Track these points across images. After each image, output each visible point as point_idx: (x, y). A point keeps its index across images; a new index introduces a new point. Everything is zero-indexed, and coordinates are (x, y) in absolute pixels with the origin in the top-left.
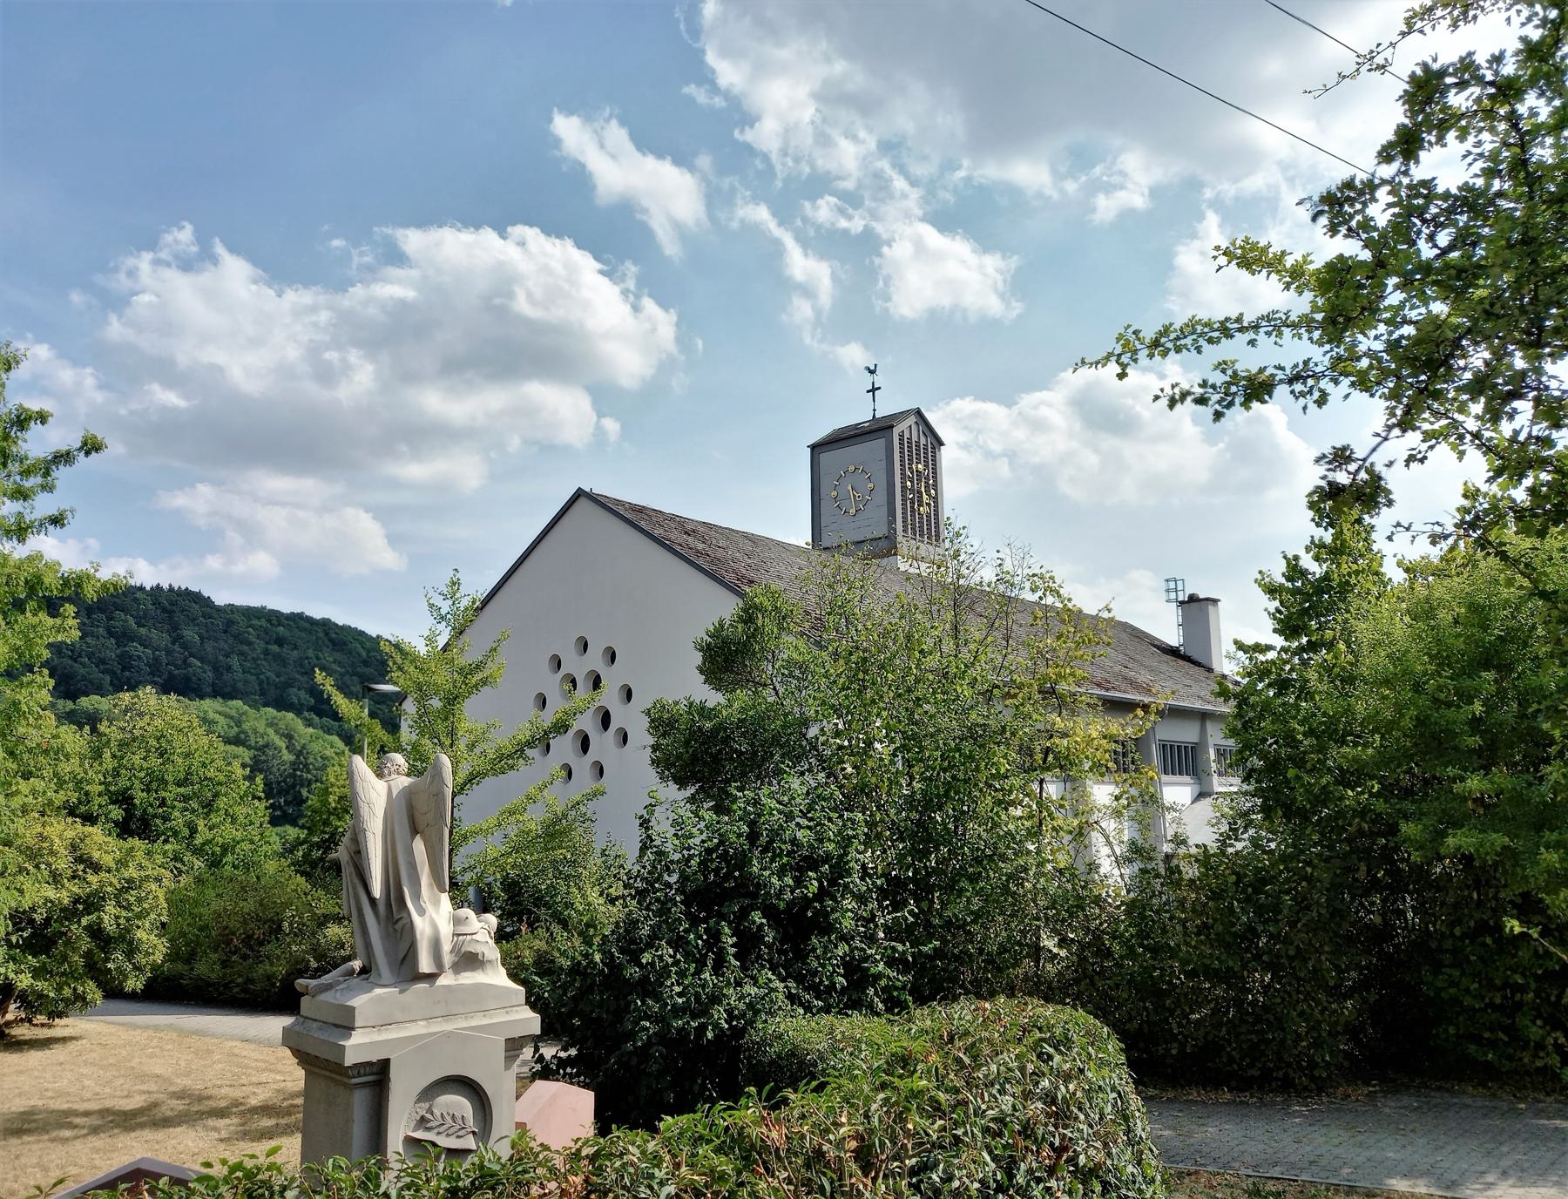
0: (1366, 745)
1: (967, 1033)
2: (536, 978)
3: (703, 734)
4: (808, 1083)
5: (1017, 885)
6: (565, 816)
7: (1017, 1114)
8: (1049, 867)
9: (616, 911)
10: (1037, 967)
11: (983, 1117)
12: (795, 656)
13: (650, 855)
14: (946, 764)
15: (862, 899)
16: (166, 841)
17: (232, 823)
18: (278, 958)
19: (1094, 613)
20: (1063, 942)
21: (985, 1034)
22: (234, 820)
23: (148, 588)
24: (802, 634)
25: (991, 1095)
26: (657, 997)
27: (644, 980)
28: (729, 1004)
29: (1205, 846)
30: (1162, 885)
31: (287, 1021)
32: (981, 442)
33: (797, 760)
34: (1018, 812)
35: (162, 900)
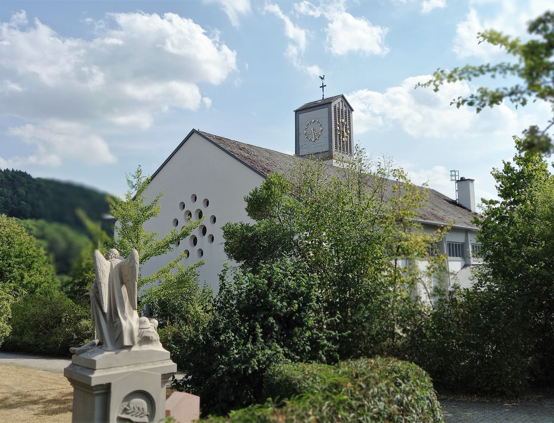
0: (538, 246)
1: (364, 374)
2: (174, 346)
3: (248, 238)
4: (295, 396)
5: (385, 306)
6: (186, 274)
7: (386, 410)
8: (399, 298)
9: (209, 317)
10: (393, 341)
11: (371, 412)
12: (288, 204)
13: (224, 292)
14: (354, 252)
15: (317, 312)
16: (11, 282)
17: (39, 274)
18: (60, 334)
19: (421, 186)
20: (405, 331)
21: (372, 374)
22: (41, 273)
23: (3, 170)
24: (291, 194)
25: (374, 402)
26: (227, 355)
27: (221, 347)
28: (258, 358)
29: (468, 289)
30: (448, 306)
31: (64, 364)
32: (370, 110)
33: (289, 250)
34: (386, 273)
35: (9, 308)
